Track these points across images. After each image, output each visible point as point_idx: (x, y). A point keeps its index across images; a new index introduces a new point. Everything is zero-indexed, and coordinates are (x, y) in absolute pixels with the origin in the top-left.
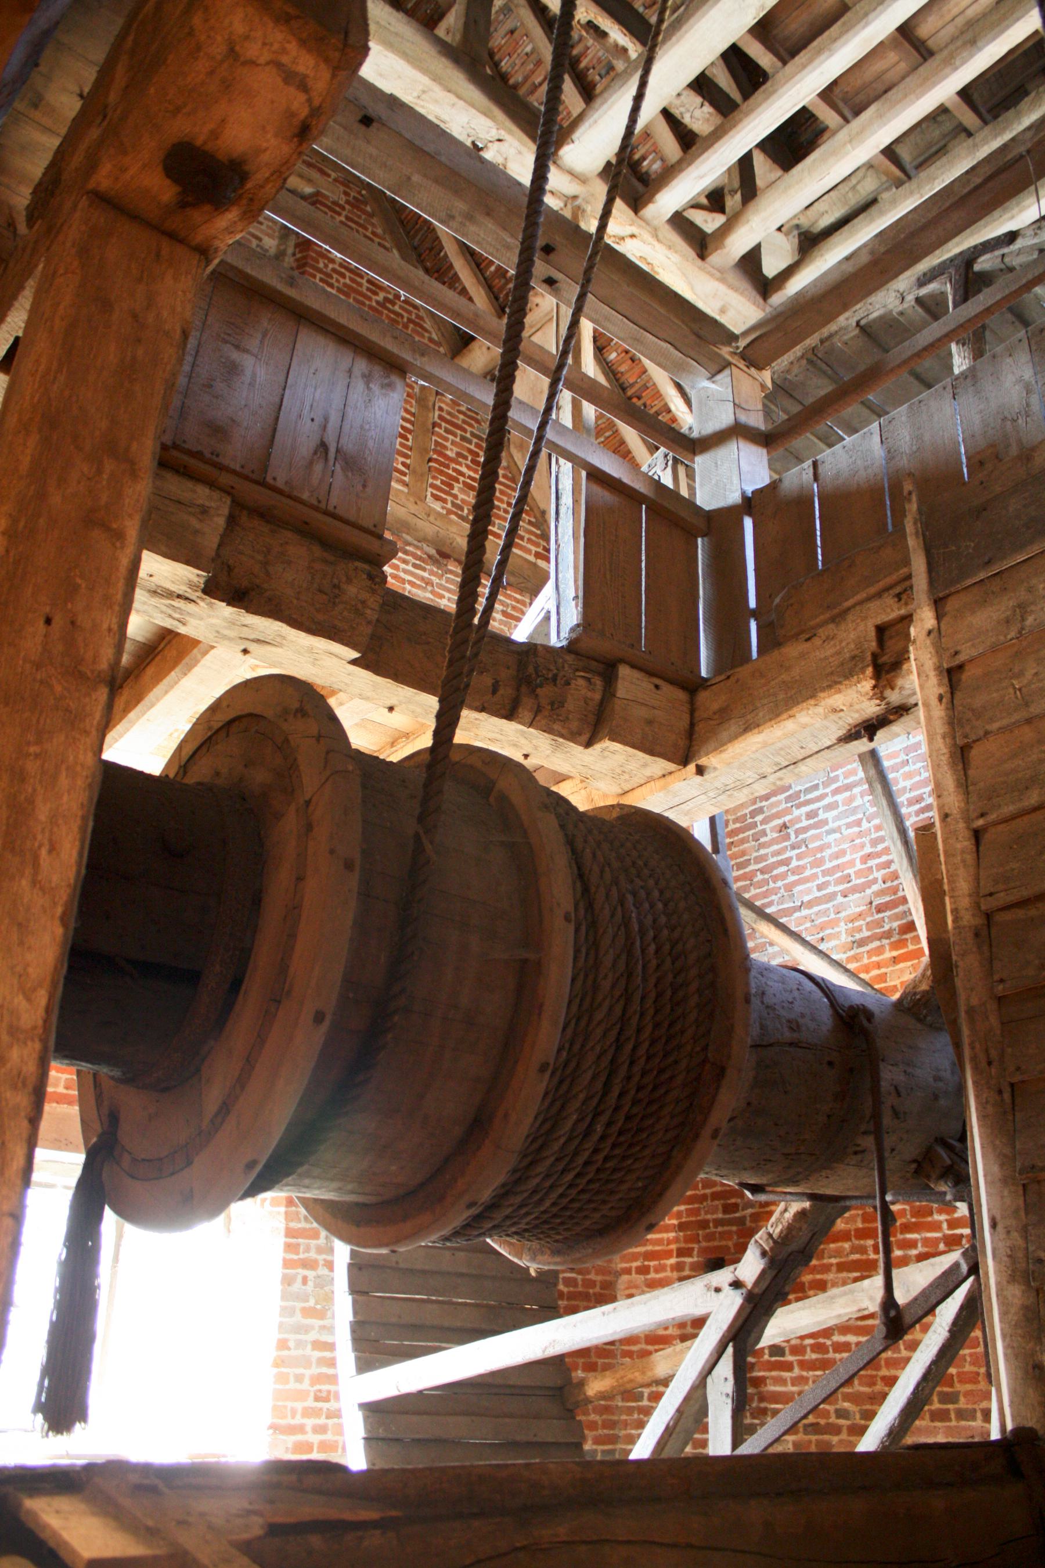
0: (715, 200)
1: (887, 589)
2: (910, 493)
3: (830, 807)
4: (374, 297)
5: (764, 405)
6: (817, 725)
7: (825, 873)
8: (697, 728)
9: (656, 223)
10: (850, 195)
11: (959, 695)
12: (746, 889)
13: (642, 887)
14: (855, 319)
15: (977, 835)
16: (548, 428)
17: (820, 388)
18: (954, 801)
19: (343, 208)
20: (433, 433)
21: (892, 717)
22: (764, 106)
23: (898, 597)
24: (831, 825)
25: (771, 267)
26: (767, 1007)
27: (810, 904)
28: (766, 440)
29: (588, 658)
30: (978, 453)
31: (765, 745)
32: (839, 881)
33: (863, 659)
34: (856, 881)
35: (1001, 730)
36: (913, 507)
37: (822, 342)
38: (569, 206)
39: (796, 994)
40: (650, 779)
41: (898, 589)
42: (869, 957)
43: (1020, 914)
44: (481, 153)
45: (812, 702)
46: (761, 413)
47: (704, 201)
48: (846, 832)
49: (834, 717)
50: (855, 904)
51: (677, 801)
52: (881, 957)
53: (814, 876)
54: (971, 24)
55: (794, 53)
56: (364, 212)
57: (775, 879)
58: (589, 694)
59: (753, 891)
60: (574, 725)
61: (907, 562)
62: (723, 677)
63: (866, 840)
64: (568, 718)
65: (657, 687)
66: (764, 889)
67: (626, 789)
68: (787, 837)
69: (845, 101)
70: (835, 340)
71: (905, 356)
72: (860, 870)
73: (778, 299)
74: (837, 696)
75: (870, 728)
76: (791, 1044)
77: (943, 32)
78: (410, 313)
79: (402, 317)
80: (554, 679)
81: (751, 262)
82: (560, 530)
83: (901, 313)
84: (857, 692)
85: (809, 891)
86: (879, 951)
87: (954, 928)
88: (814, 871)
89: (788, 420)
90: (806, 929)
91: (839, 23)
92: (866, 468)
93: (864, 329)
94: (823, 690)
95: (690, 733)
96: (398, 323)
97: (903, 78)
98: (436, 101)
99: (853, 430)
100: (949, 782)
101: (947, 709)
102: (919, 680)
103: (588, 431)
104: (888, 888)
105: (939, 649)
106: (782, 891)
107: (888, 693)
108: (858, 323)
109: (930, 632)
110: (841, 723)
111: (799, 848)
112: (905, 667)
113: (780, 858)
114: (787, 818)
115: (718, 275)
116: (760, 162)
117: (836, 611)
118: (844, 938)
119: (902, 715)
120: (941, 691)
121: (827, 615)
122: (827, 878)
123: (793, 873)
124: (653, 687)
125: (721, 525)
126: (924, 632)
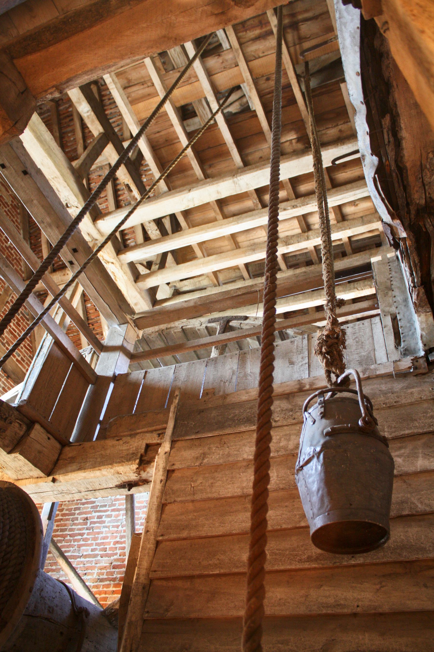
0: (149, 265)
1: (156, 430)
2: (177, 396)
3: (109, 516)
4: (5, 244)
5: (136, 342)
6: (109, 477)
7: (97, 544)
8: (59, 462)
9: (123, 262)
10: (197, 283)
11: (169, 482)
12: (60, 541)
13: (2, 522)
14: (182, 325)
15: (158, 543)
16: (45, 316)
17: (159, 345)
18: (153, 526)
19: (8, 206)
20: (5, 305)
21: (140, 483)
22: (177, 238)
23: (159, 435)
24: (106, 524)
25: (160, 296)
26: (42, 597)
27: (85, 556)
28: (132, 356)
29: (24, 415)
30: (207, 390)
31: (85, 478)
32: (101, 550)
33: (137, 455)
34: (108, 552)
35: (181, 502)
36: (176, 401)
37: (167, 329)
38: (93, 242)
39: (58, 594)
40: (31, 477)
41: (160, 432)
42: (103, 588)
43: (164, 583)
44: (68, 209)
45: (110, 466)
46: (133, 346)
47: (145, 264)
48: (111, 529)
49: (117, 475)
50: (105, 562)
51: (39, 491)
52: (108, 589)
53: (92, 545)
54: (254, 244)
55: (194, 226)
56: (16, 212)
57: (75, 541)
58: (18, 431)
59: (63, 543)
60: (7, 442)
61: (166, 422)
62: (78, 444)
63: (118, 535)
64: (5, 438)
65: (49, 438)
66: (68, 544)
67: (19, 478)
68: (86, 524)
69: (206, 250)
70: (172, 330)
71: (194, 345)
72: (112, 547)
73: (157, 307)
74: (121, 467)
75: (130, 485)
76: (46, 619)
77: (245, 243)
78: (17, 255)
79: (13, 256)
80: (6, 419)
81: (153, 291)
82: (37, 361)
83: (199, 330)
84: (130, 468)
85: (87, 550)
86: (108, 586)
87: (135, 582)
88: (93, 542)
89: (143, 352)
90: (80, 567)
91: (212, 224)
92: (165, 381)
93: (183, 330)
94: (116, 463)
95: (56, 463)
96: (10, 257)
97: (228, 251)
98: (59, 183)
99: (166, 364)
100: (154, 517)
101: (162, 486)
102: (155, 472)
103: (64, 327)
104: (121, 559)
105: (167, 461)
106: (76, 547)
107: (142, 472)
108: (182, 327)
109: (166, 453)
110: (119, 479)
111: (90, 530)
112: (152, 464)
113: (80, 532)
114: (89, 515)
115: (139, 290)
116: (170, 257)
117: (133, 432)
118: (95, 576)
119: (145, 484)
120: (163, 478)
121: (129, 433)
122: (97, 547)
123: (83, 540)
124: (47, 437)
125: (101, 383)
126: (164, 452)
